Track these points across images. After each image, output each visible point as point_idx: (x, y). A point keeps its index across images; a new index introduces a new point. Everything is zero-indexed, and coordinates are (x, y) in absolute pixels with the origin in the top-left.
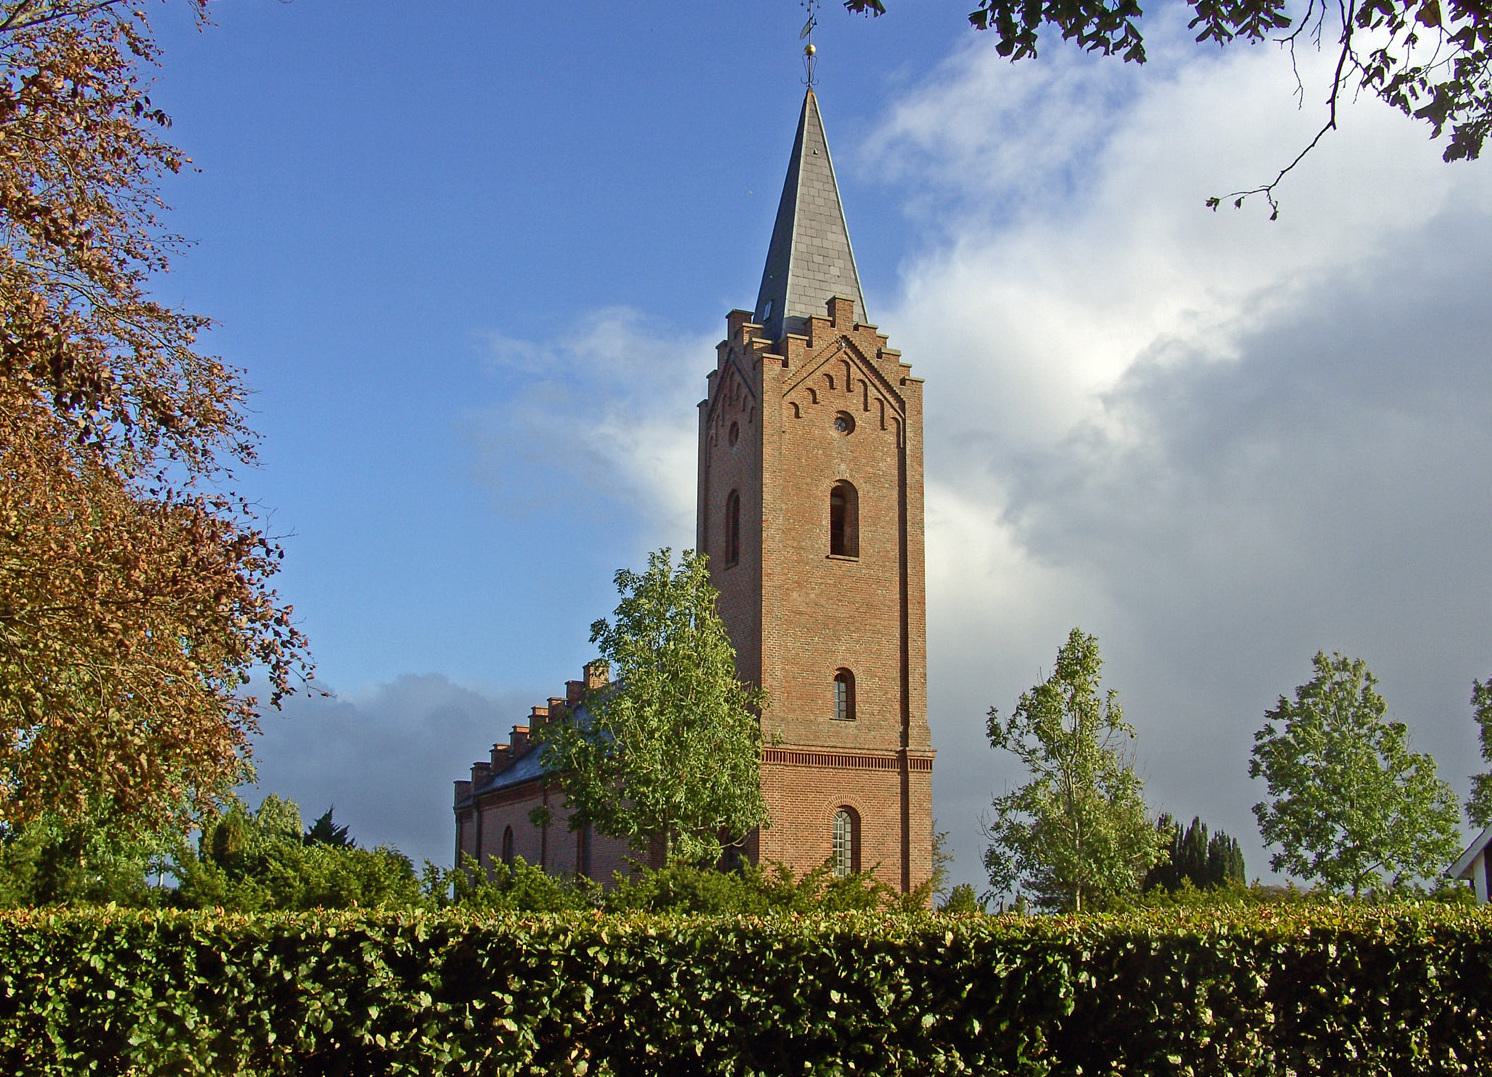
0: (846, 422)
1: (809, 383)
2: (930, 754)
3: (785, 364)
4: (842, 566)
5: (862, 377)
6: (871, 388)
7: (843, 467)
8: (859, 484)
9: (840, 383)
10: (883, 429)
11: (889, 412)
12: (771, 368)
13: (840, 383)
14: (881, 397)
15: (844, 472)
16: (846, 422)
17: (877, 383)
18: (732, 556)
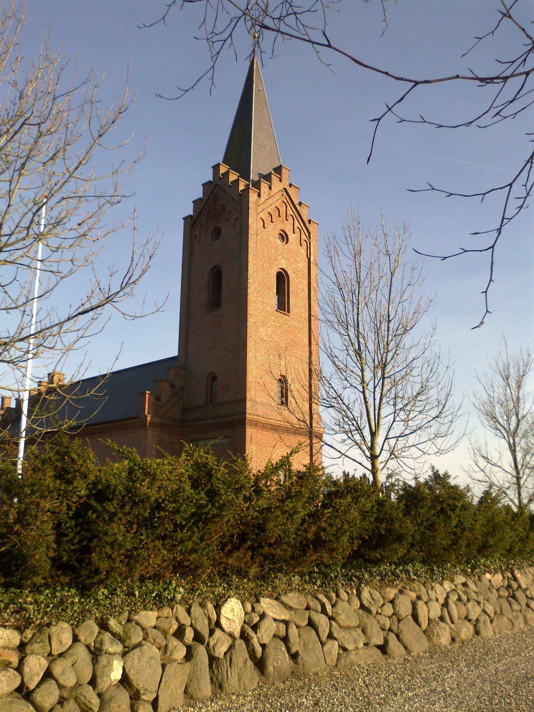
0: (284, 237)
1: (269, 210)
2: (322, 430)
3: (259, 196)
4: (281, 316)
5: (293, 214)
6: (296, 222)
7: (283, 261)
8: (290, 272)
9: (283, 213)
10: (294, 233)
11: (304, 237)
12: (253, 196)
13: (283, 213)
14: (293, 214)
15: (283, 264)
16: (284, 237)
17: (300, 221)
18: (217, 275)
